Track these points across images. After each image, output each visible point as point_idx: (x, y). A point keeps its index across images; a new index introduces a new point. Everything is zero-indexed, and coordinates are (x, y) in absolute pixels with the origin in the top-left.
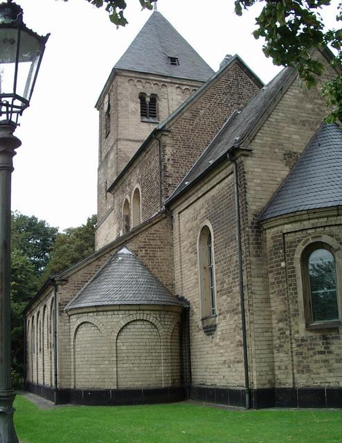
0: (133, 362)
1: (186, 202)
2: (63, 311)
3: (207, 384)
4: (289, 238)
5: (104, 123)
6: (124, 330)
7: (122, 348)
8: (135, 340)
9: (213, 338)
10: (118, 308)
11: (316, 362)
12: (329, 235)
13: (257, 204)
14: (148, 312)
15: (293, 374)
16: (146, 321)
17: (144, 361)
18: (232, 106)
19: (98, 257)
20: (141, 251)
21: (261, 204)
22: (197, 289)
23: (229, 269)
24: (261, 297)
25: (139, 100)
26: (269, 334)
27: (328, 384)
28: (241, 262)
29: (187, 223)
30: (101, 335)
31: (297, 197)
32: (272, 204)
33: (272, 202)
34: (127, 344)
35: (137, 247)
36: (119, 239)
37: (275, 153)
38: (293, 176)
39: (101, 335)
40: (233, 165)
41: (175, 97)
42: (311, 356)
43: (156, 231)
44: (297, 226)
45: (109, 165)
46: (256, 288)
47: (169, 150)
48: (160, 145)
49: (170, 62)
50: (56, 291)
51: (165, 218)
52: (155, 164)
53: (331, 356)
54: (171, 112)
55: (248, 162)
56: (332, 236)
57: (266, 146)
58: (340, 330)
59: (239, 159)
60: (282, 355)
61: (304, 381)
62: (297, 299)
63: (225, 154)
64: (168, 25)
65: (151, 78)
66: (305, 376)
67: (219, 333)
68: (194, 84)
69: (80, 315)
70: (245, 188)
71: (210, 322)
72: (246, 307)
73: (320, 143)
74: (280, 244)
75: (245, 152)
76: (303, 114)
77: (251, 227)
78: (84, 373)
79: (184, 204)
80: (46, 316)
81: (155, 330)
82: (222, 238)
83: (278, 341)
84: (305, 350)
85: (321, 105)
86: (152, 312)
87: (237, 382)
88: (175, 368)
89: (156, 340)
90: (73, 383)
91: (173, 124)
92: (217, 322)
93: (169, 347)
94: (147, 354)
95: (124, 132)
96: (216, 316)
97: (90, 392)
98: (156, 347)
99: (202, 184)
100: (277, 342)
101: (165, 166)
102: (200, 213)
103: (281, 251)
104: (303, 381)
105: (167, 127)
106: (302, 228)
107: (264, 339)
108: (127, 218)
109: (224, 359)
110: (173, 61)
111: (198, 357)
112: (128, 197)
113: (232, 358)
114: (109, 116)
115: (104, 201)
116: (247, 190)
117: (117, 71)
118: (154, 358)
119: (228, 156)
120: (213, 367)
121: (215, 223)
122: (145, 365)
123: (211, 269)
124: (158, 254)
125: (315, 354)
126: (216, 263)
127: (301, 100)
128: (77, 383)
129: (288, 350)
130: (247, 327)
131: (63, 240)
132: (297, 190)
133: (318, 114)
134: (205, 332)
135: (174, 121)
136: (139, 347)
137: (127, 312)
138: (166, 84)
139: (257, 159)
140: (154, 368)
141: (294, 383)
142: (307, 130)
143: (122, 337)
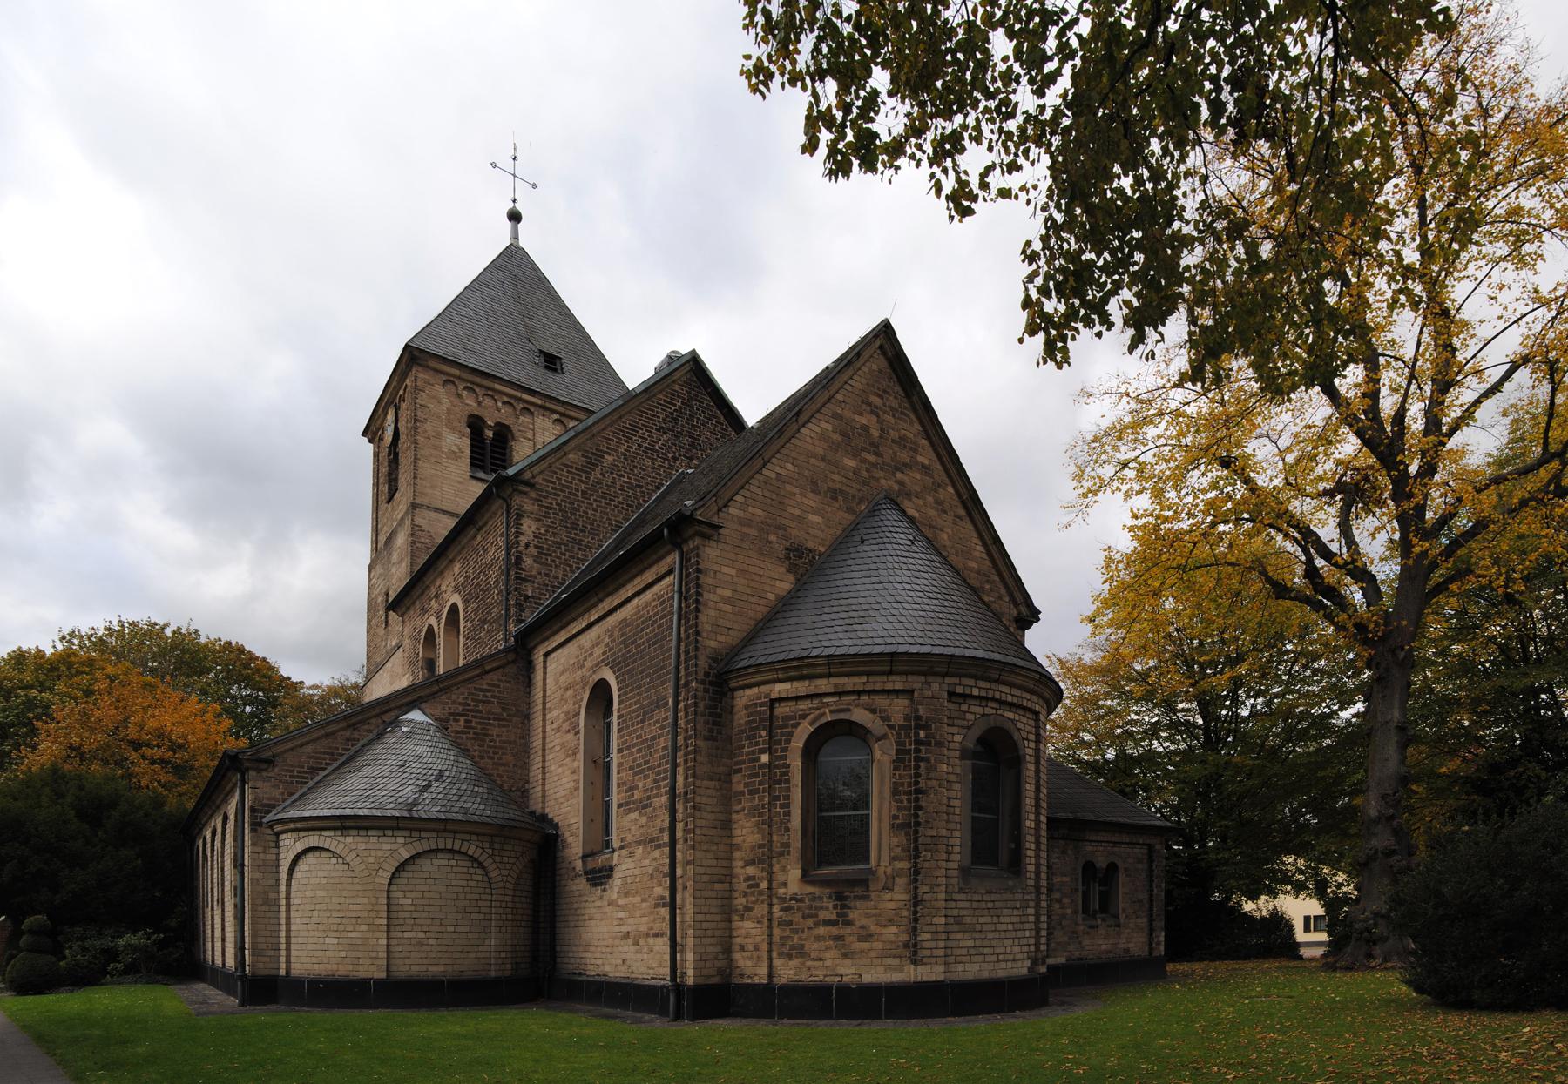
0: (425, 928)
1: (563, 632)
2: (260, 824)
4: (782, 710)
5: (384, 470)
8: (434, 888)
9: (604, 890)
11: (818, 938)
15: (770, 959)
16: (459, 852)
17: (452, 929)
18: (675, 459)
19: (354, 720)
21: (729, 639)
22: (574, 801)
23: (647, 763)
24: (712, 817)
25: (468, 430)
28: (675, 749)
29: (562, 673)
31: (808, 632)
34: (414, 894)
35: (447, 711)
38: (799, 594)
42: (809, 929)
43: (494, 685)
45: (395, 557)
46: (704, 800)
47: (529, 526)
48: (508, 512)
50: (243, 782)
53: (848, 930)
55: (708, 550)
56: (873, 711)
60: (748, 924)
61: (791, 972)
63: (659, 530)
64: (540, 283)
65: (497, 386)
66: (795, 962)
67: (618, 882)
69: (302, 834)
70: (697, 602)
71: (601, 860)
72: (679, 834)
73: (865, 537)
74: (761, 720)
75: (704, 529)
76: (836, 477)
77: (702, 682)
78: (309, 947)
81: (479, 871)
82: (636, 703)
83: (743, 900)
84: (797, 917)
85: (875, 465)
87: (651, 972)
89: (482, 891)
90: (283, 966)
92: (615, 862)
93: (510, 905)
94: (460, 916)
95: (429, 491)
96: (614, 851)
97: (322, 982)
98: (480, 904)
99: (600, 596)
100: (740, 901)
101: (519, 560)
102: (592, 654)
103: (764, 733)
104: (788, 972)
105: (527, 475)
106: (812, 690)
107: (713, 894)
109: (625, 929)
110: (551, 362)
111: (572, 924)
112: (433, 621)
113: (643, 928)
114: (396, 455)
115: (381, 631)
116: (701, 607)
117: (415, 353)
118: (477, 923)
119: (666, 531)
120: (601, 943)
122: (455, 936)
123: (607, 767)
124: (495, 731)
125: (817, 924)
126: (620, 751)
128: (293, 966)
129: (763, 916)
130: (679, 871)
131: (305, 705)
132: (809, 619)
133: (865, 483)
134: (588, 880)
135: (544, 465)
136: (443, 902)
137: (416, 834)
138: (532, 409)
139: (728, 548)
140: (472, 942)
141: (770, 976)
143: (404, 881)
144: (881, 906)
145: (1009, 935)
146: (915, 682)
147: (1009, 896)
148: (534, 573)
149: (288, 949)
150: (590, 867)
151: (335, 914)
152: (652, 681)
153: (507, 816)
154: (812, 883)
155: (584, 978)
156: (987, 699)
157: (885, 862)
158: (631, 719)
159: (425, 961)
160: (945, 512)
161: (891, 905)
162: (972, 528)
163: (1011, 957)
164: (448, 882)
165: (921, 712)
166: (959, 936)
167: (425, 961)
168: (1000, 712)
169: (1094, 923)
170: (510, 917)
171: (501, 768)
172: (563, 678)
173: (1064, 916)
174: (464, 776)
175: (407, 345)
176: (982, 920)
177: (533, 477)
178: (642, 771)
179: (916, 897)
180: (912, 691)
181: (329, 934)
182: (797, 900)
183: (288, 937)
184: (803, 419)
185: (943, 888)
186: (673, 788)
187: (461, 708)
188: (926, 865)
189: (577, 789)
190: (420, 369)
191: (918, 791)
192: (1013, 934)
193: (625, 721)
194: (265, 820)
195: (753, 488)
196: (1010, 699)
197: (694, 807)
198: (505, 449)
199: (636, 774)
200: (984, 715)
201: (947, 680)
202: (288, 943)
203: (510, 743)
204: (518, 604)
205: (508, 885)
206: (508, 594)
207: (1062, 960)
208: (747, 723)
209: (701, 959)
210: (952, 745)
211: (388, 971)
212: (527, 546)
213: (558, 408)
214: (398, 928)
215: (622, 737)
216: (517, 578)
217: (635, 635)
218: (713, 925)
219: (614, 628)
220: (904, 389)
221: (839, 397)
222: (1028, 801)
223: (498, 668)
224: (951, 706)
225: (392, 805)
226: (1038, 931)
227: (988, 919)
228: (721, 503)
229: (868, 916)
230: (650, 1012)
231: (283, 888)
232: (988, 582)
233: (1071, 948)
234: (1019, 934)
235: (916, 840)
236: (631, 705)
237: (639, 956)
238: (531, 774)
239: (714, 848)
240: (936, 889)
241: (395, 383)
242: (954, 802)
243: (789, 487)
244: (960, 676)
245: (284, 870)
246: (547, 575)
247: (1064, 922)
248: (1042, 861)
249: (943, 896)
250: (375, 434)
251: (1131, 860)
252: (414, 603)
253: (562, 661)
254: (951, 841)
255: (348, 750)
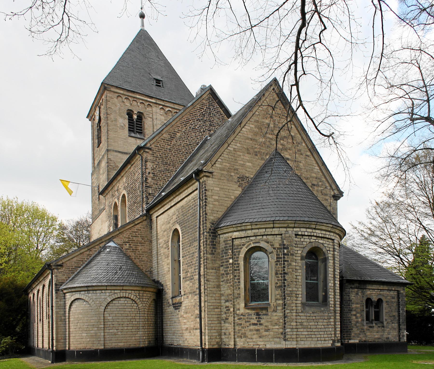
2: (58, 290)
3: (175, 344)
4: (236, 242)
5: (96, 133)
6: (110, 305)
7: (109, 318)
8: (119, 312)
9: (179, 311)
10: (105, 288)
11: (251, 330)
12: (265, 242)
13: (215, 215)
14: (130, 292)
15: (235, 338)
16: (128, 298)
17: (126, 328)
18: (204, 131)
19: (90, 247)
20: (126, 245)
21: (218, 215)
23: (192, 262)
24: (214, 283)
25: (127, 116)
26: (219, 310)
27: (258, 346)
28: (200, 258)
29: (163, 225)
30: (91, 308)
32: (226, 216)
33: (227, 214)
35: (123, 241)
36: (109, 233)
37: (232, 176)
39: (91, 308)
40: (197, 183)
41: (159, 117)
42: (248, 326)
43: (139, 230)
44: (242, 234)
45: (101, 171)
46: (210, 277)
47: (149, 165)
48: (142, 159)
49: (155, 83)
51: (146, 220)
52: (138, 175)
54: (155, 130)
56: (268, 242)
57: (224, 170)
58: (268, 309)
59: (202, 179)
60: (227, 325)
62: (240, 286)
63: (191, 175)
65: (138, 96)
66: (243, 339)
67: (184, 308)
68: (176, 107)
69: (74, 293)
72: (202, 290)
74: (229, 246)
75: (207, 174)
77: (208, 232)
78: (77, 337)
79: (160, 210)
80: (45, 294)
81: (135, 305)
82: (188, 239)
83: (225, 315)
84: (243, 322)
86: (133, 292)
87: (195, 343)
88: (151, 332)
89: (136, 312)
91: (154, 143)
92: (182, 300)
94: (129, 323)
95: (113, 144)
96: (182, 296)
98: (136, 318)
99: (174, 196)
100: (224, 316)
101: (146, 179)
102: (172, 218)
103: (230, 251)
104: (241, 344)
105: (148, 145)
107: (214, 313)
108: (116, 218)
111: (169, 325)
112: (116, 200)
113: (192, 326)
114: (100, 127)
115: (97, 202)
116: (207, 204)
117: (106, 86)
118: (135, 325)
121: (183, 227)
122: (127, 331)
124: (140, 248)
125: (250, 325)
126: (183, 257)
127: (256, 134)
129: (232, 322)
130: (203, 304)
134: (174, 307)
135: (154, 140)
137: (113, 291)
138: (151, 104)
139: (216, 180)
141: (235, 345)
142: (258, 159)
144: (273, 318)
145: (322, 330)
146: (283, 230)
147: (322, 314)
148: (152, 184)
149: (69, 339)
150: (174, 302)
151: (86, 324)
152: (192, 231)
153: (144, 283)
154: (248, 309)
155: (173, 346)
156: (311, 236)
157: (273, 301)
158: (186, 245)
159: (117, 341)
160: (302, 154)
161: (276, 318)
162: (313, 159)
163: (323, 339)
164: (124, 310)
165: (285, 242)
166: (302, 330)
167: (117, 341)
168: (317, 241)
169: (371, 325)
170: (147, 322)
171: (142, 262)
172: (163, 227)
173: (357, 322)
174: (129, 267)
175: (102, 83)
176: (310, 324)
177: (151, 145)
178: (190, 265)
179: (285, 314)
180: (282, 234)
181: (83, 332)
182: (243, 316)
183: (69, 334)
184: (242, 125)
185: (295, 311)
186: (199, 273)
187: (127, 240)
188: (288, 302)
189: (169, 271)
190: (108, 92)
191: (285, 273)
192: (324, 330)
193: (184, 245)
194: (60, 288)
195: (224, 155)
196: (320, 235)
197: (207, 280)
198: (141, 122)
199: (188, 266)
200: (310, 242)
201: (295, 229)
202: (69, 337)
203: (145, 252)
204: (147, 197)
205: (145, 310)
206: (143, 193)
207: (357, 341)
208: (225, 247)
209: (210, 339)
210: (297, 255)
211: (104, 346)
212: (149, 173)
213: (162, 103)
214: (108, 328)
215: (183, 252)
216: (146, 186)
217: (186, 212)
218: (214, 325)
219: (179, 209)
220: (283, 105)
221: (257, 113)
222: (330, 275)
223: (140, 223)
224: (296, 239)
225: (105, 281)
226: (335, 328)
227: (313, 323)
228: (213, 163)
229: (268, 322)
230: (194, 359)
231: (67, 315)
232: (320, 181)
233: (361, 336)
234: (327, 330)
235: (284, 292)
236: (186, 240)
237: (191, 337)
238: (153, 265)
239: (214, 295)
240: (292, 311)
241: (98, 97)
242: (298, 277)
243: (238, 153)
244: (300, 228)
245: (67, 307)
246: (157, 184)
247: (358, 325)
248: (337, 300)
249: (294, 314)
250: (92, 117)
251: (389, 298)
252: (109, 192)
253: (163, 220)
254: (298, 293)
255: (88, 259)
